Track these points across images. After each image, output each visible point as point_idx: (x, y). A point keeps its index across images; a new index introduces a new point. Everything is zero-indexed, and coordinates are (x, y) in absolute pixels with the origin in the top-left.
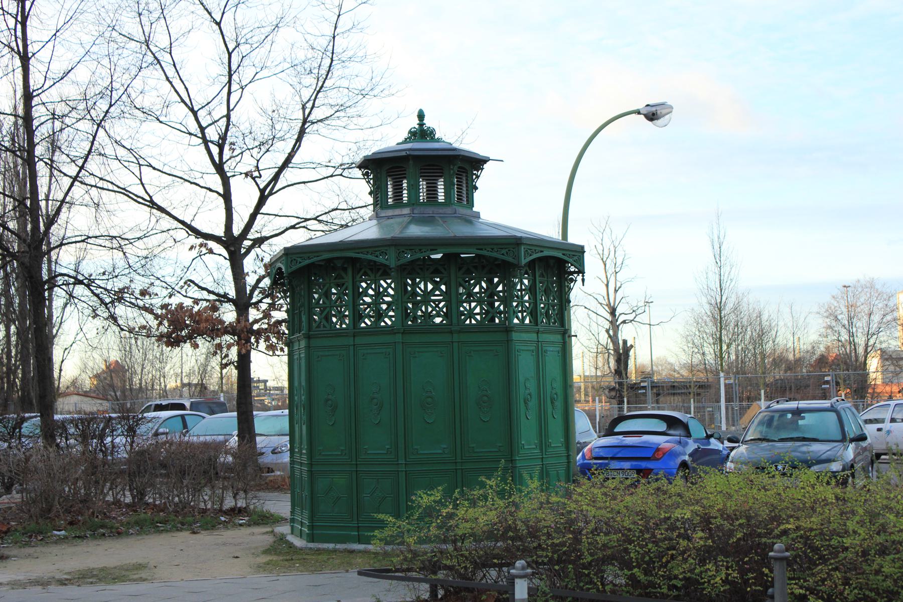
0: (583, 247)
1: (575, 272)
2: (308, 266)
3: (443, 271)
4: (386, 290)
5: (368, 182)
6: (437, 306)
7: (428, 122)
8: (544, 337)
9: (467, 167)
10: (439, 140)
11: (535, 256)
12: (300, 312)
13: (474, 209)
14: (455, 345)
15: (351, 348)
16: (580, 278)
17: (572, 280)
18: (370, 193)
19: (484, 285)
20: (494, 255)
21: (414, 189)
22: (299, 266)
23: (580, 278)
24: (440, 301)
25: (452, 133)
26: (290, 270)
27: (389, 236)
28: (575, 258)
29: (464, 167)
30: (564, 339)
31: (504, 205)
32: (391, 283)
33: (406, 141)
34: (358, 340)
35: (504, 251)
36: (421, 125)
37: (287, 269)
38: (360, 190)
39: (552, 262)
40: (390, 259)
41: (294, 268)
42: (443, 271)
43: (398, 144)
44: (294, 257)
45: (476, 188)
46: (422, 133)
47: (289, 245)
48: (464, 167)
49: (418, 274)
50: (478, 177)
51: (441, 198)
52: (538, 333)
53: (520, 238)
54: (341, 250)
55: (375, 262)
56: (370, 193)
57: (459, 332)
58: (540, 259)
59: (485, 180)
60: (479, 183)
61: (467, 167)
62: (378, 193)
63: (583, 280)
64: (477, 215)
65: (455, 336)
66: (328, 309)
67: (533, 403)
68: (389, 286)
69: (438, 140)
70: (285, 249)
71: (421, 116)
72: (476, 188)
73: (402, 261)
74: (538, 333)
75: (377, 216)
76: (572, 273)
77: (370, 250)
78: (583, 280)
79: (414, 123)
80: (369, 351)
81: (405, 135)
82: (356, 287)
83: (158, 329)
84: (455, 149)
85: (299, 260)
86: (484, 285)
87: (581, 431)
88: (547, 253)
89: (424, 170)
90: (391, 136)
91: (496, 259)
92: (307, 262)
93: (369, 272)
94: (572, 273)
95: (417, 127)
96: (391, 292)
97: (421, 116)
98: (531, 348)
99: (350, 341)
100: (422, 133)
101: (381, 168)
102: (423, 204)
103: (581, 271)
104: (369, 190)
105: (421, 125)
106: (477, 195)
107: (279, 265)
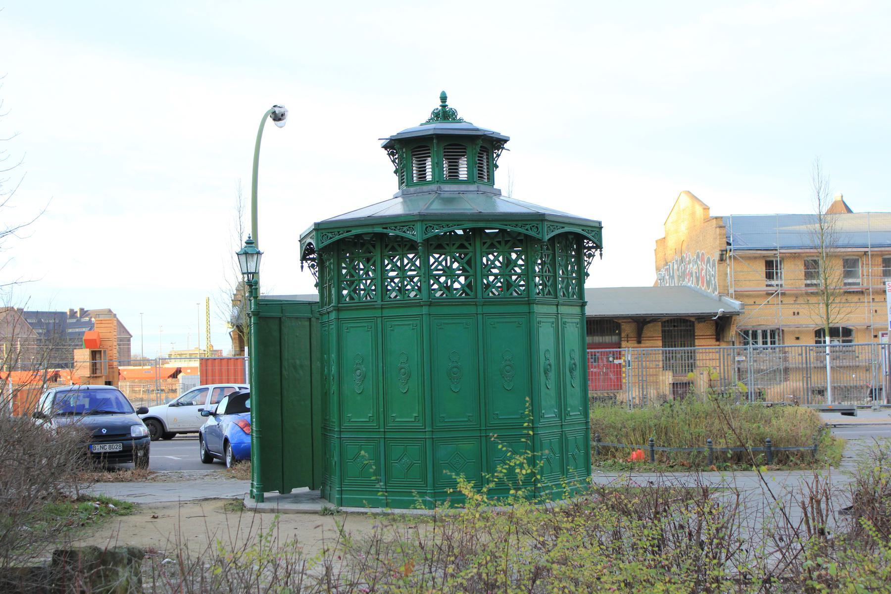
0: (600, 223)
1: (593, 247)
2: (338, 241)
3: (468, 246)
4: (493, 262)
5: (394, 161)
6: (412, 280)
7: (450, 104)
8: (562, 309)
9: (488, 146)
10: (460, 121)
11: (557, 232)
12: (330, 286)
13: (495, 187)
14: (480, 317)
15: (379, 320)
17: (590, 256)
18: (396, 172)
20: (519, 229)
21: (437, 166)
22: (329, 242)
23: (598, 253)
24: (414, 277)
25: (475, 116)
26: (321, 246)
27: (416, 212)
28: (593, 234)
29: (486, 147)
31: (523, 184)
32: (434, 257)
33: (428, 122)
34: (386, 313)
35: (405, 229)
36: (444, 106)
37: (317, 244)
38: (385, 167)
39: (570, 237)
40: (416, 234)
41: (326, 243)
42: (468, 246)
43: (422, 125)
44: (324, 232)
45: (497, 167)
46: (444, 114)
47: (319, 220)
48: (486, 147)
49: (497, 248)
51: (429, 177)
52: (557, 305)
53: (544, 215)
54: (373, 225)
55: (402, 237)
57: (484, 304)
58: (559, 235)
59: (504, 159)
60: (499, 162)
61: (488, 146)
62: (402, 172)
63: (601, 255)
64: (498, 193)
65: (480, 308)
66: (356, 282)
67: (552, 375)
68: (496, 258)
69: (460, 121)
70: (315, 224)
71: (444, 98)
72: (497, 167)
73: (429, 235)
74: (557, 305)
75: (404, 195)
76: (589, 248)
77: (520, 224)
78: (601, 255)
80: (446, 321)
81: (428, 116)
82: (383, 262)
84: (478, 130)
85: (330, 235)
88: (567, 229)
89: (448, 149)
90: (415, 118)
91: (520, 234)
92: (337, 238)
93: (398, 248)
94: (589, 248)
95: (440, 108)
96: (497, 264)
97: (444, 98)
98: (551, 320)
99: (378, 313)
100: (444, 114)
101: (406, 149)
102: (430, 183)
103: (599, 246)
104: (394, 169)
105: (444, 106)
106: (497, 174)
107: (309, 240)
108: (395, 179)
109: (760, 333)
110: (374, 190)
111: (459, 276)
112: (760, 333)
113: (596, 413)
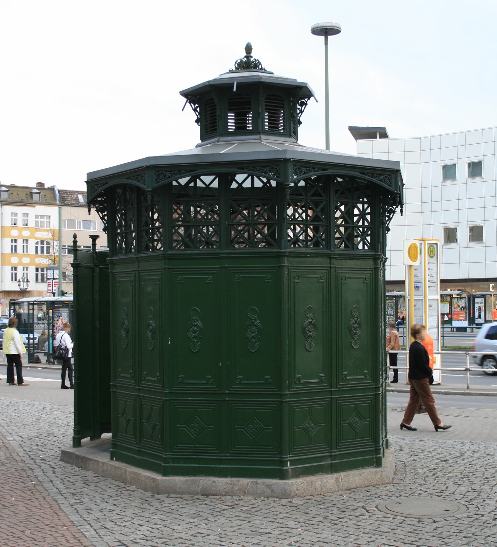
0: (399, 162)
7: (255, 55)
16: (398, 210)
18: (197, 121)
19: (310, 233)
30: (376, 263)
36: (248, 57)
38: (189, 118)
45: (300, 123)
46: (248, 64)
50: (302, 112)
56: (197, 121)
63: (402, 211)
71: (249, 49)
72: (300, 123)
78: (402, 211)
79: (242, 55)
83: (317, 480)
86: (310, 233)
87: (324, 147)
89: (247, 101)
90: (218, 67)
97: (249, 49)
100: (248, 64)
104: (196, 118)
108: (197, 128)
109: (39, 280)
110: (179, 135)
111: (179, 226)
112: (39, 280)
113: (286, 258)
